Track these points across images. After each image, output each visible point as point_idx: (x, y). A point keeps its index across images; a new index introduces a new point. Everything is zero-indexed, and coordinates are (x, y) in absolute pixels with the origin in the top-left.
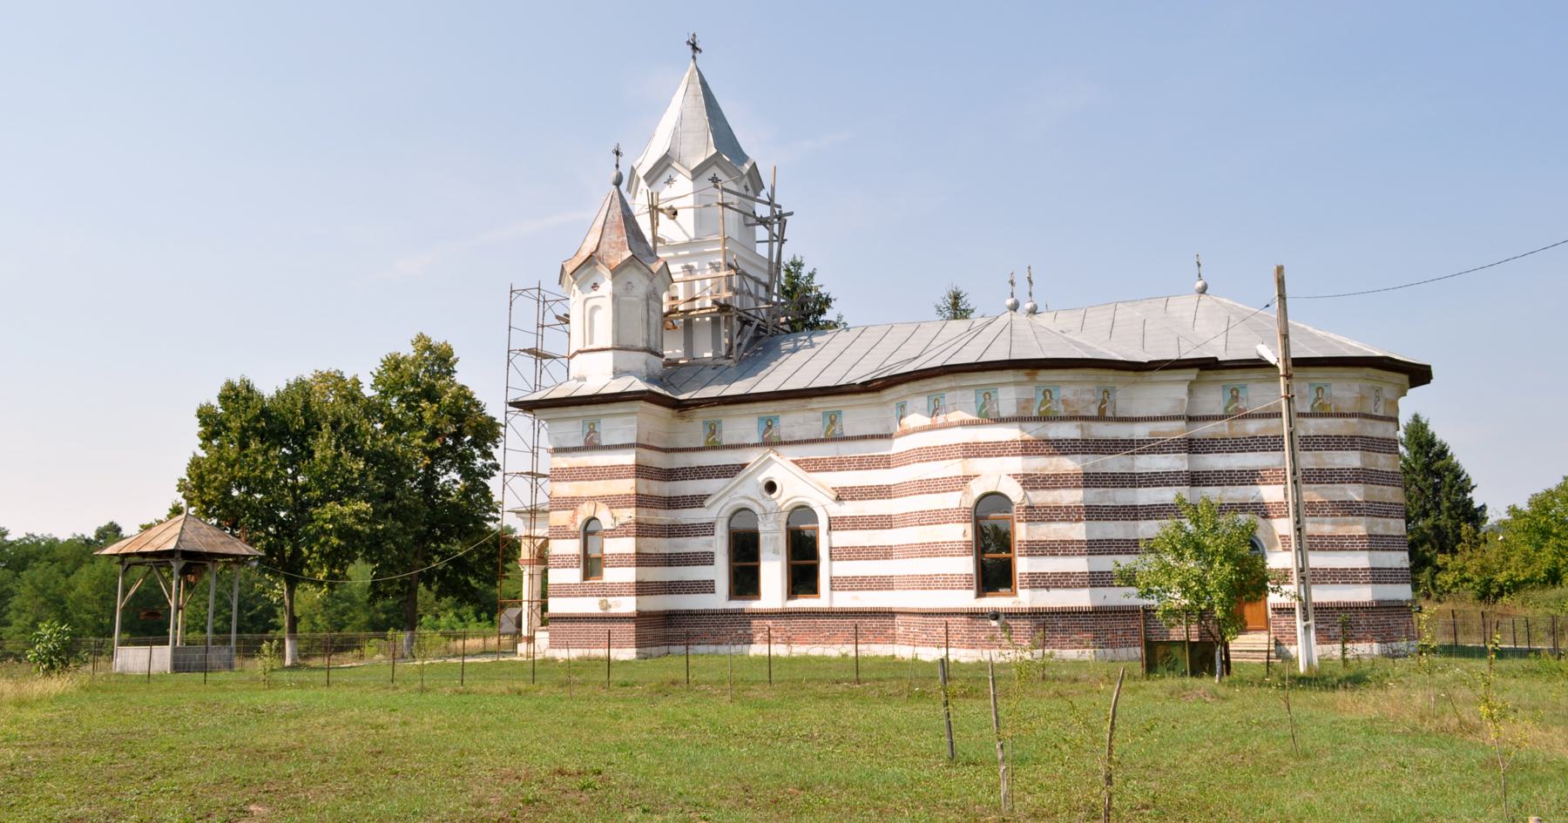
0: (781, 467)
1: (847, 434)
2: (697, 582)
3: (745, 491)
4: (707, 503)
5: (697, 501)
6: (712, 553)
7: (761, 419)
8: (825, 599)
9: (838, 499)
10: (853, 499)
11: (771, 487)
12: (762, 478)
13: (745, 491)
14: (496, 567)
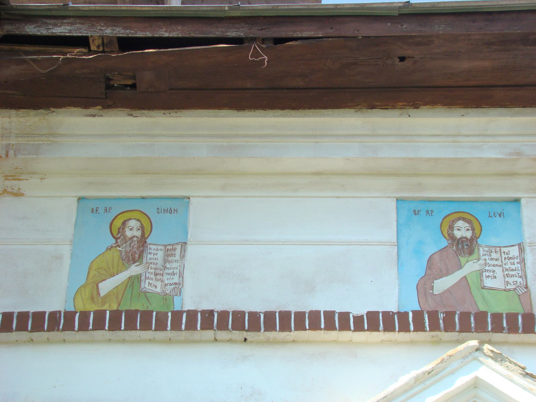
7: (412, 209)
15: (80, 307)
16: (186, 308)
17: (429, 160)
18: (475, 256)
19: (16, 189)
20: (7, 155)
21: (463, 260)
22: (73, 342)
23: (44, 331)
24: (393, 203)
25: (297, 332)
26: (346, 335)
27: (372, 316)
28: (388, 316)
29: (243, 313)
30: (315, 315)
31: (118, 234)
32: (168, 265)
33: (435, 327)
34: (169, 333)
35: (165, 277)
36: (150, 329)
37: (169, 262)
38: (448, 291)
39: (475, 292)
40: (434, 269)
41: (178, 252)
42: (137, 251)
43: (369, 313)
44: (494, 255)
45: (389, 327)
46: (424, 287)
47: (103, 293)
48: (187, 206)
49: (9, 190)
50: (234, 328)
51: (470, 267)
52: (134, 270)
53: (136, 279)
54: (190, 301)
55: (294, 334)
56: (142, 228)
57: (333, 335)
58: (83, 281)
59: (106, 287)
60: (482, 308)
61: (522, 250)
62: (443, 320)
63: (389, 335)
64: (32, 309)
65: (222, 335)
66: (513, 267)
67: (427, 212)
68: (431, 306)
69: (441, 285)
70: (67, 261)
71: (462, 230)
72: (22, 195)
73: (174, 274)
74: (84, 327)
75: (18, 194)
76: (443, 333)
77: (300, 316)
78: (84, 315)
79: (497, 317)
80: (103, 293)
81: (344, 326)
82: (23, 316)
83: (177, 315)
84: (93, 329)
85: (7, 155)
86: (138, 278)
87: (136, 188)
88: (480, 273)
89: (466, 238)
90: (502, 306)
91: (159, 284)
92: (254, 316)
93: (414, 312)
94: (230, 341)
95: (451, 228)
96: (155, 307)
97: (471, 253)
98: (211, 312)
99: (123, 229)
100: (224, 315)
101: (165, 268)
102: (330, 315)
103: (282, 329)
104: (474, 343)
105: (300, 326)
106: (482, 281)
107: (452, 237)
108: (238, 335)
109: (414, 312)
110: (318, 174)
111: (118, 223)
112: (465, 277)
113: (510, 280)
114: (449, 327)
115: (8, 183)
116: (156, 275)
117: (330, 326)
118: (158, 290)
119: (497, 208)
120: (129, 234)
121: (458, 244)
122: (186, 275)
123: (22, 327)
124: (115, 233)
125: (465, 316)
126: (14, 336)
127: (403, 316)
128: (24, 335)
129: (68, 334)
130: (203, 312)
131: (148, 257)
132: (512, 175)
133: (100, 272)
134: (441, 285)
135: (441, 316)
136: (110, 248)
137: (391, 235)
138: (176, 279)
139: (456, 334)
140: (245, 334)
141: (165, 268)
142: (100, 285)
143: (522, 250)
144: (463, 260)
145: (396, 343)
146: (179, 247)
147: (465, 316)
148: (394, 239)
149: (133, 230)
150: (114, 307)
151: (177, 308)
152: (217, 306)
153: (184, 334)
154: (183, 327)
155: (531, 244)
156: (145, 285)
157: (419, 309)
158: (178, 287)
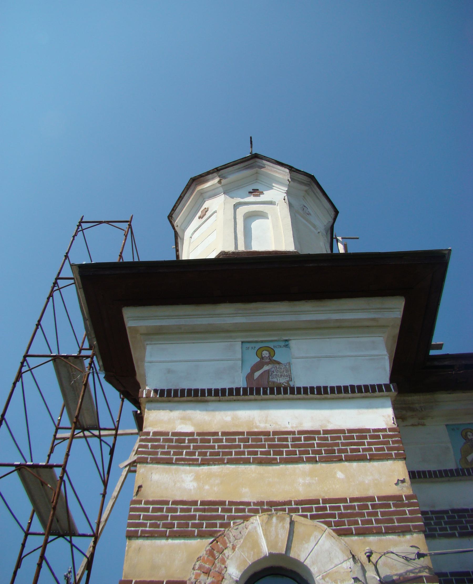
75: (423, 425)
111: (464, 433)
136: (465, 443)
142: (467, 458)
157: (246, 386)
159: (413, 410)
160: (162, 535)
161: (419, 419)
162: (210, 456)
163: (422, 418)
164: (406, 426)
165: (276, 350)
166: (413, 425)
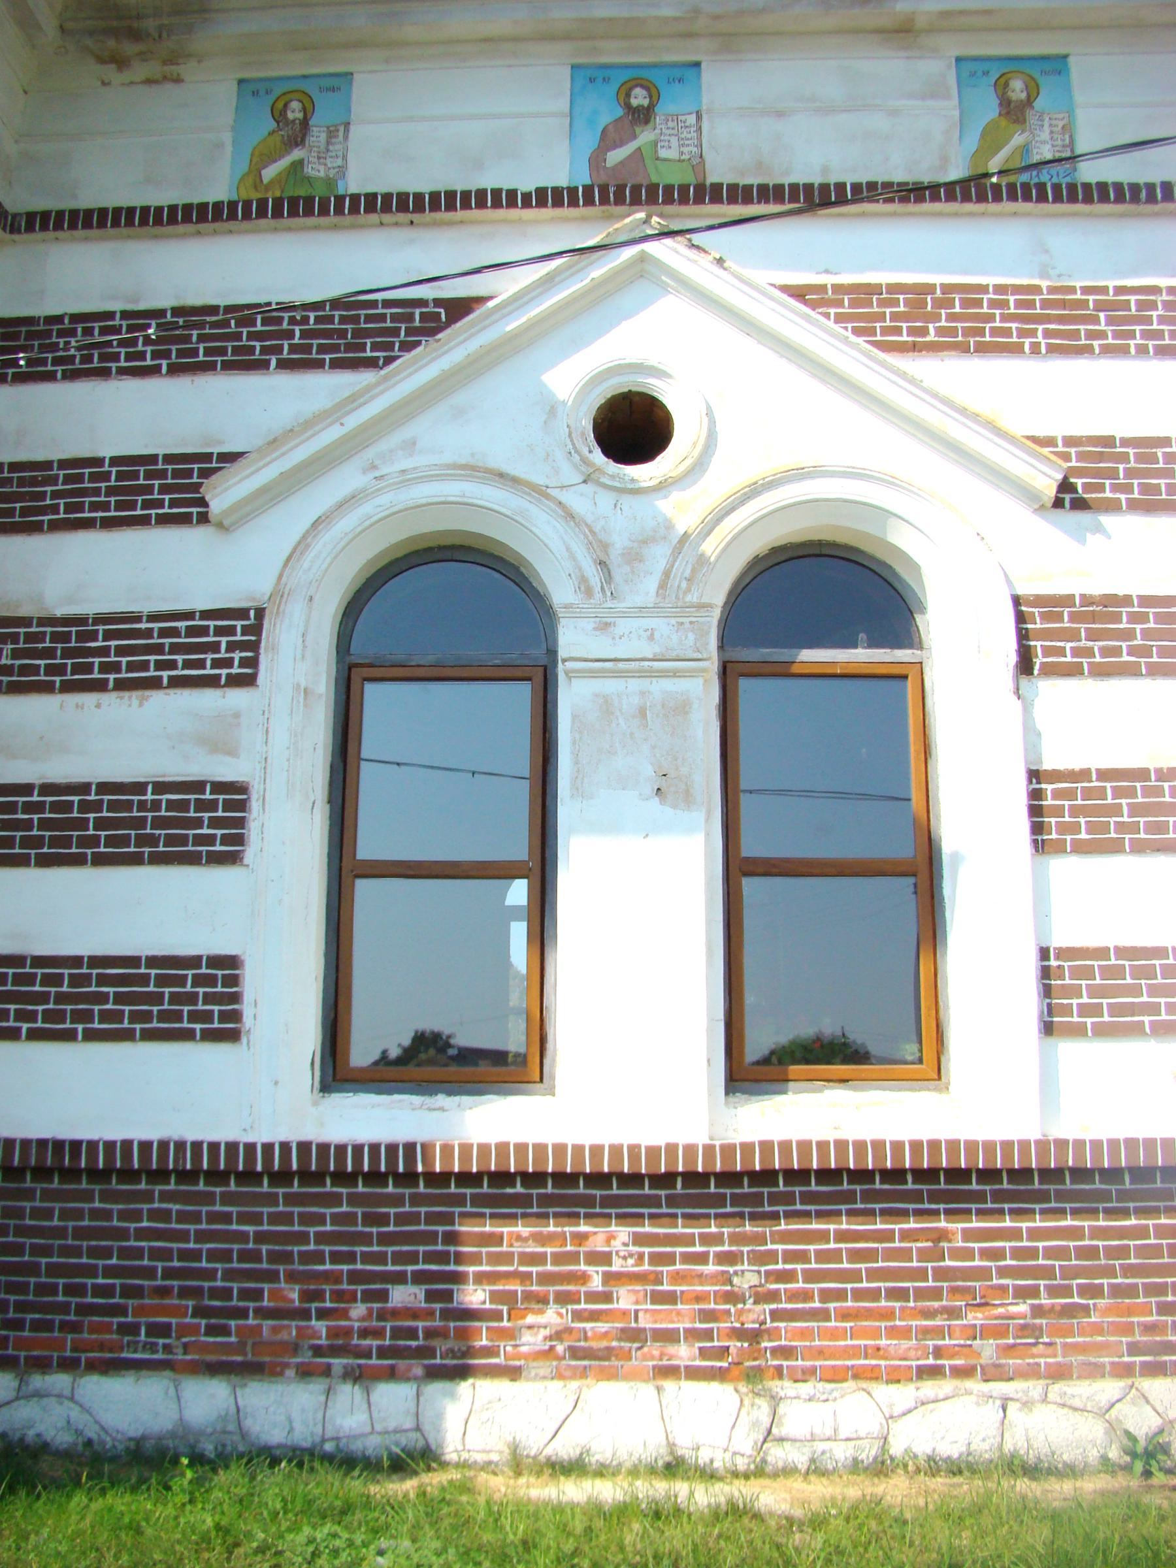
0: (708, 321)
1: (719, 173)
2: (119, 969)
3: (479, 439)
4: (222, 495)
5: (167, 489)
6: (235, 795)
7: (588, 76)
8: (994, 1081)
9: (1068, 499)
10: (1148, 506)
11: (632, 428)
12: (575, 379)
13: (479, 439)
14: (755, 1376)
15: (244, 196)
16: (349, 192)
17: (603, 20)
18: (651, 125)
19: (175, 74)
20: (160, 36)
21: (638, 130)
22: (240, 232)
23: (222, 220)
24: (567, 71)
25: (463, 212)
26: (514, 213)
27: (541, 192)
28: (557, 192)
29: (408, 195)
30: (481, 194)
31: (279, 115)
32: (331, 148)
33: (604, 201)
34: (332, 219)
35: (328, 161)
36: (313, 215)
37: (333, 144)
38: (622, 163)
39: (648, 162)
40: (608, 141)
41: (341, 134)
42: (298, 135)
43: (538, 190)
44: (670, 124)
45: (558, 203)
46: (596, 160)
47: (266, 180)
48: (351, 83)
49: (169, 76)
50: (398, 210)
51: (645, 137)
52: (297, 154)
53: (298, 165)
54: (355, 183)
55: (460, 214)
56: (304, 109)
57: (501, 213)
58: (246, 169)
59: (269, 173)
60: (655, 180)
61: (699, 117)
62: (613, 191)
63: (558, 212)
64: (196, 200)
65: (387, 218)
66: (689, 136)
67: (604, 79)
68: (603, 179)
69: (615, 157)
70: (229, 148)
71: (639, 98)
72: (182, 81)
73: (337, 157)
74: (247, 216)
75: (178, 80)
76: (614, 207)
77: (466, 195)
78: (247, 204)
79: (669, 189)
80: (266, 180)
81: (512, 203)
82: (188, 208)
83: (340, 199)
84: (257, 218)
85: (160, 36)
86: (301, 163)
87: (295, 66)
88: (655, 144)
89: (642, 106)
90: (674, 177)
91: (322, 168)
92: (419, 197)
93: (584, 187)
94: (396, 224)
95: (628, 95)
96: (318, 192)
97: (647, 122)
98: (375, 195)
99: (285, 112)
100: (387, 197)
101: (328, 150)
102: (496, 193)
103: (448, 209)
104: (641, 215)
105: (466, 205)
106: (656, 152)
107: (628, 106)
108: (403, 217)
109: (584, 187)
110: (487, 40)
111: (280, 105)
112: (639, 149)
113: (686, 150)
114: (620, 200)
115: (166, 68)
116: (319, 158)
117: (497, 204)
118: (322, 174)
119: (677, 73)
120: (290, 116)
121: (633, 114)
122: (351, 156)
123: (187, 219)
124: (277, 114)
125: (636, 189)
126: (181, 228)
127: (573, 191)
128: (190, 228)
129: (232, 225)
130: (367, 195)
131: (311, 140)
132: (690, 35)
133: (263, 158)
134: (615, 157)
135: (612, 190)
136: (271, 134)
137: (563, 104)
138: (339, 162)
139: (627, 208)
140: (410, 216)
141: (328, 150)
142: (264, 172)
143: (699, 117)
144: (638, 130)
145: (566, 220)
146: (342, 129)
147: (636, 189)
148: (567, 110)
149: (295, 112)
150: (278, 194)
151: (341, 192)
152: (380, 188)
153: (348, 219)
154: (346, 211)
155: (709, 111)
156: (309, 170)
157: (589, 182)
158: (342, 171)
159: (136, 35)
160: (211, 682)
161: (165, 63)
162: (226, 347)
163: (172, 60)
164: (132, 83)
165: (1042, 80)
166: (149, 82)
